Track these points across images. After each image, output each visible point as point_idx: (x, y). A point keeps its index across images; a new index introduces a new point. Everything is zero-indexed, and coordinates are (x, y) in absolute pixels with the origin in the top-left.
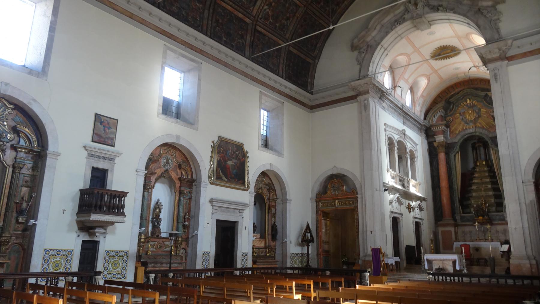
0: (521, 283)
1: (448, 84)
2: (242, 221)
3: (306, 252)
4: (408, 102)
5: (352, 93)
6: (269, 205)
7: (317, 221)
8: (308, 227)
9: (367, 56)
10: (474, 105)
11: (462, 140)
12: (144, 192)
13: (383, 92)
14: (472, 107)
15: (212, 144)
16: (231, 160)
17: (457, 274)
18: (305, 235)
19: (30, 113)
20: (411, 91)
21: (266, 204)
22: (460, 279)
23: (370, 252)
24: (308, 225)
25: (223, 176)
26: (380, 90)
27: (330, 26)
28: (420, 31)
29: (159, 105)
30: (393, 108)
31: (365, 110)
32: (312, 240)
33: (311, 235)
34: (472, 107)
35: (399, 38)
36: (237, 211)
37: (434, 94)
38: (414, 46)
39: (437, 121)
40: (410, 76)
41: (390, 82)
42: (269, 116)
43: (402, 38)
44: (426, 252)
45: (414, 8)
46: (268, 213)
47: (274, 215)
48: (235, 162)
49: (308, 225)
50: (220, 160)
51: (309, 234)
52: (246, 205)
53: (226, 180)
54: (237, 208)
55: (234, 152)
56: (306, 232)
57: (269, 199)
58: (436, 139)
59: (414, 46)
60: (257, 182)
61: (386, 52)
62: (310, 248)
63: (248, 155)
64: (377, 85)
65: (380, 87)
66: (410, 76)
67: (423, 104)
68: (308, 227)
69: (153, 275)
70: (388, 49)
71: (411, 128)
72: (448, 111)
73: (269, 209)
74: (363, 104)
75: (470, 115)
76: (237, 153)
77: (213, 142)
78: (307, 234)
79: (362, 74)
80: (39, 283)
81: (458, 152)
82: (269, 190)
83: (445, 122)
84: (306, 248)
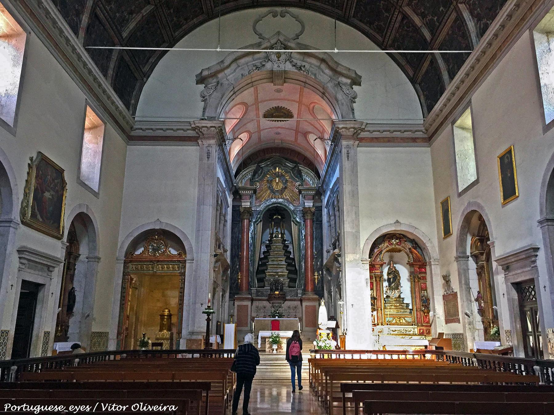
1: (264, 146)
2: (50, 285)
5: (191, 133)
9: (215, 93)
10: (282, 175)
11: (266, 209)
12: (479, 282)
14: (280, 176)
15: (30, 162)
16: (49, 191)
19: (184, 143)
22: (338, 357)
25: (38, 213)
29: (489, 220)
31: (208, 158)
34: (280, 176)
36: (46, 269)
37: (247, 153)
39: (245, 184)
45: (276, 59)
48: (52, 195)
50: (37, 187)
52: (56, 261)
53: (41, 220)
55: (53, 180)
58: (243, 204)
67: (237, 162)
69: (16, 367)
71: (546, 254)
74: (206, 150)
75: (278, 185)
76: (56, 181)
77: (31, 159)
79: (207, 114)
80: (346, 358)
81: (261, 221)
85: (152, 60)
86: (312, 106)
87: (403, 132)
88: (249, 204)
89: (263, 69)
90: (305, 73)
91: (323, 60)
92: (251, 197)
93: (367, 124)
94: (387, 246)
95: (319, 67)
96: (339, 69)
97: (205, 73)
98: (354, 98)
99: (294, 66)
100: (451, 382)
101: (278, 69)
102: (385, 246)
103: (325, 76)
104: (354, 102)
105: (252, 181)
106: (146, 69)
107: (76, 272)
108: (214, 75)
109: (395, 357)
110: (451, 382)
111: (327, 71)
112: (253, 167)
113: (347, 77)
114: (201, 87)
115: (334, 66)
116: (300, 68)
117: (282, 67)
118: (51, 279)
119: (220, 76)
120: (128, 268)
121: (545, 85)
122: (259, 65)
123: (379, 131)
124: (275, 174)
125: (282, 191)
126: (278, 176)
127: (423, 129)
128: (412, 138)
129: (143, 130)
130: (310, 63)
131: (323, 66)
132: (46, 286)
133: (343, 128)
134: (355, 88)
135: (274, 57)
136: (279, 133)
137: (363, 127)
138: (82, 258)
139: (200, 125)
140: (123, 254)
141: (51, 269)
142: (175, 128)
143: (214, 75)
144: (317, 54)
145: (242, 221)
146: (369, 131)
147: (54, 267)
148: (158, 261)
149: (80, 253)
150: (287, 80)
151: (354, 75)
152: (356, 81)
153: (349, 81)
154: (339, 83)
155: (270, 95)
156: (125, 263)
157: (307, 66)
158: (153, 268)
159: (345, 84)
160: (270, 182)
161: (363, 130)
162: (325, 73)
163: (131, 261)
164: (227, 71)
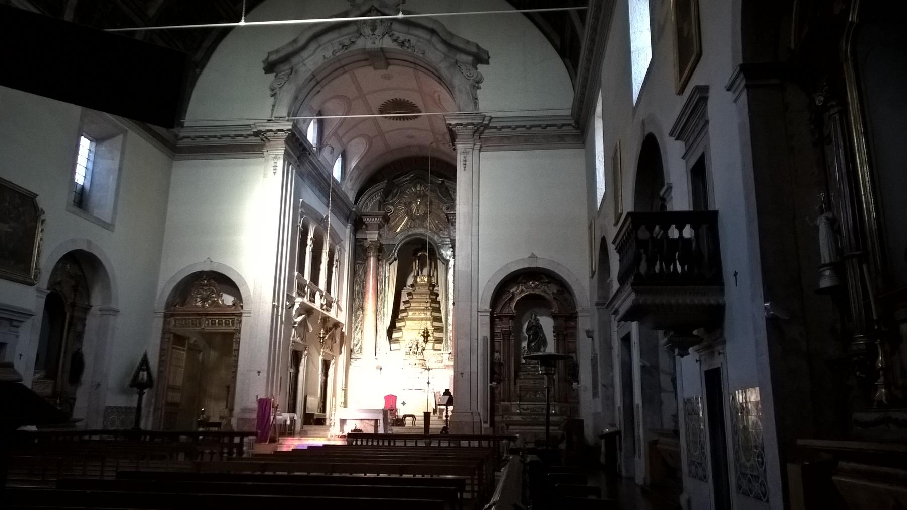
0: (447, 445)
3: (135, 404)
4: (337, 173)
6: (72, 317)
7: (162, 350)
8: (145, 362)
13: (305, 149)
14: (423, 196)
17: (375, 436)
18: (137, 373)
20: (342, 157)
21: (65, 314)
23: (255, 405)
24: (145, 356)
26: (301, 144)
27: (239, 20)
28: (371, 68)
30: (314, 178)
32: (149, 383)
33: (149, 375)
35: (341, 71)
38: (359, 88)
39: (372, 209)
40: (346, 133)
41: (316, 135)
42: (93, 149)
43: (345, 72)
44: (500, 401)
45: (371, 33)
46: (69, 330)
47: (80, 336)
49: (145, 356)
51: (145, 373)
52: (28, 315)
54: (8, 317)
56: (140, 369)
57: (73, 305)
59: (359, 88)
60: (56, 269)
61: (318, 88)
62: (144, 397)
63: (43, 217)
64: (298, 136)
65: (301, 140)
66: (346, 133)
67: (357, 179)
68: (145, 362)
70: (322, 83)
72: (390, 197)
73: (70, 324)
78: (141, 373)
81: (395, 259)
82: (75, 289)
83: (382, 212)
84: (136, 397)
85: (207, 44)
86: (436, 95)
87: (514, 129)
88: (377, 236)
89: (353, 48)
90: (410, 50)
91: (433, 31)
92: (380, 227)
93: (491, 118)
94: (522, 291)
95: (429, 41)
96: (455, 42)
97: (273, 58)
98: (478, 82)
99: (395, 40)
100: (309, 473)
101: (373, 46)
102: (519, 292)
103: (435, 54)
104: (479, 88)
105: (382, 204)
106: (199, 56)
107: (86, 328)
108: (286, 59)
109: (410, 443)
110: (309, 473)
111: (440, 46)
112: (383, 185)
113: (468, 53)
114: (271, 76)
115: (448, 38)
116: (402, 44)
117: (379, 44)
118: (17, 337)
119: (295, 60)
120: (169, 323)
121: (637, 49)
122: (347, 42)
123: (510, 127)
124: (415, 193)
125: (424, 217)
126: (419, 197)
127: (572, 122)
128: (559, 136)
129: (232, 138)
130: (419, 37)
131: (435, 40)
132: (8, 347)
133: (457, 125)
134: (481, 68)
135: (367, 31)
136: (412, 137)
137: (486, 122)
138: (95, 310)
139: (263, 129)
140: (163, 305)
141: (15, 323)
142: (232, 134)
143: (286, 59)
144: (420, 21)
145: (366, 260)
146: (495, 128)
147: (21, 322)
148: (207, 315)
149: (92, 304)
150: (391, 61)
151: (474, 50)
152: (480, 58)
153: (470, 59)
154: (456, 62)
155: (379, 84)
156: (166, 316)
157: (413, 41)
158: (200, 324)
159: (465, 63)
160: (408, 205)
161: (487, 127)
162: (437, 49)
163: (173, 315)
164: (304, 54)
